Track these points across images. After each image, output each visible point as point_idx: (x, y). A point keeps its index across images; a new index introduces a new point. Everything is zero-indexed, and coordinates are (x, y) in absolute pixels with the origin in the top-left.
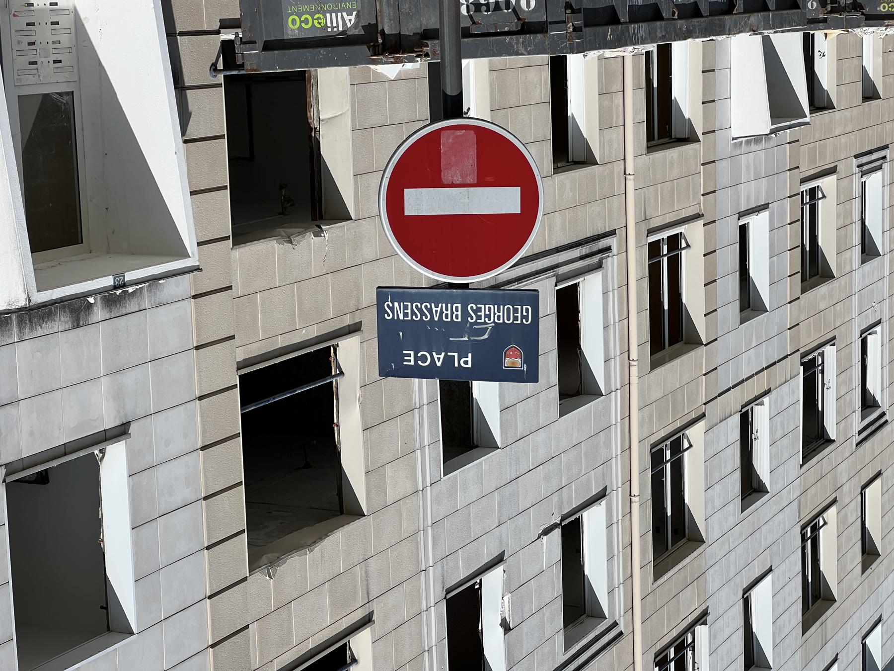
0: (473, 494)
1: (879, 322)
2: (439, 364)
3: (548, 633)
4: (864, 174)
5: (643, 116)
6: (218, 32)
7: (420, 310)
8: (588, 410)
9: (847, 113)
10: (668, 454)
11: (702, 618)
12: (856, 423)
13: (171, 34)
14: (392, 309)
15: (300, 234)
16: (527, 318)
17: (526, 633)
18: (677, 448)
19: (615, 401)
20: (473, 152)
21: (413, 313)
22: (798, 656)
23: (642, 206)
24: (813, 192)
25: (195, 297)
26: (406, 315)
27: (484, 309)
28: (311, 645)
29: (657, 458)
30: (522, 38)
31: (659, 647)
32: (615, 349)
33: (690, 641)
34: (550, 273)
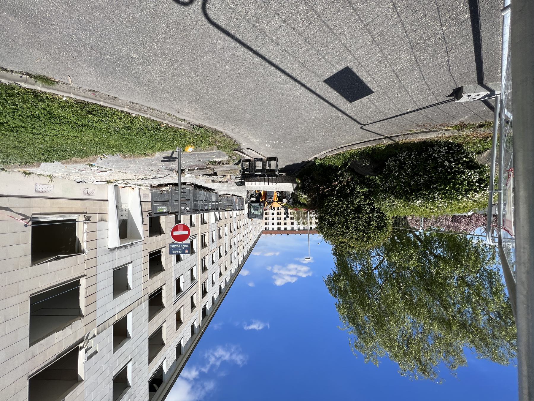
0: (179, 266)
3: (189, 282)
11: (207, 279)
13: (142, 212)
17: (186, 283)
18: (204, 259)
27: (183, 246)
29: (202, 260)
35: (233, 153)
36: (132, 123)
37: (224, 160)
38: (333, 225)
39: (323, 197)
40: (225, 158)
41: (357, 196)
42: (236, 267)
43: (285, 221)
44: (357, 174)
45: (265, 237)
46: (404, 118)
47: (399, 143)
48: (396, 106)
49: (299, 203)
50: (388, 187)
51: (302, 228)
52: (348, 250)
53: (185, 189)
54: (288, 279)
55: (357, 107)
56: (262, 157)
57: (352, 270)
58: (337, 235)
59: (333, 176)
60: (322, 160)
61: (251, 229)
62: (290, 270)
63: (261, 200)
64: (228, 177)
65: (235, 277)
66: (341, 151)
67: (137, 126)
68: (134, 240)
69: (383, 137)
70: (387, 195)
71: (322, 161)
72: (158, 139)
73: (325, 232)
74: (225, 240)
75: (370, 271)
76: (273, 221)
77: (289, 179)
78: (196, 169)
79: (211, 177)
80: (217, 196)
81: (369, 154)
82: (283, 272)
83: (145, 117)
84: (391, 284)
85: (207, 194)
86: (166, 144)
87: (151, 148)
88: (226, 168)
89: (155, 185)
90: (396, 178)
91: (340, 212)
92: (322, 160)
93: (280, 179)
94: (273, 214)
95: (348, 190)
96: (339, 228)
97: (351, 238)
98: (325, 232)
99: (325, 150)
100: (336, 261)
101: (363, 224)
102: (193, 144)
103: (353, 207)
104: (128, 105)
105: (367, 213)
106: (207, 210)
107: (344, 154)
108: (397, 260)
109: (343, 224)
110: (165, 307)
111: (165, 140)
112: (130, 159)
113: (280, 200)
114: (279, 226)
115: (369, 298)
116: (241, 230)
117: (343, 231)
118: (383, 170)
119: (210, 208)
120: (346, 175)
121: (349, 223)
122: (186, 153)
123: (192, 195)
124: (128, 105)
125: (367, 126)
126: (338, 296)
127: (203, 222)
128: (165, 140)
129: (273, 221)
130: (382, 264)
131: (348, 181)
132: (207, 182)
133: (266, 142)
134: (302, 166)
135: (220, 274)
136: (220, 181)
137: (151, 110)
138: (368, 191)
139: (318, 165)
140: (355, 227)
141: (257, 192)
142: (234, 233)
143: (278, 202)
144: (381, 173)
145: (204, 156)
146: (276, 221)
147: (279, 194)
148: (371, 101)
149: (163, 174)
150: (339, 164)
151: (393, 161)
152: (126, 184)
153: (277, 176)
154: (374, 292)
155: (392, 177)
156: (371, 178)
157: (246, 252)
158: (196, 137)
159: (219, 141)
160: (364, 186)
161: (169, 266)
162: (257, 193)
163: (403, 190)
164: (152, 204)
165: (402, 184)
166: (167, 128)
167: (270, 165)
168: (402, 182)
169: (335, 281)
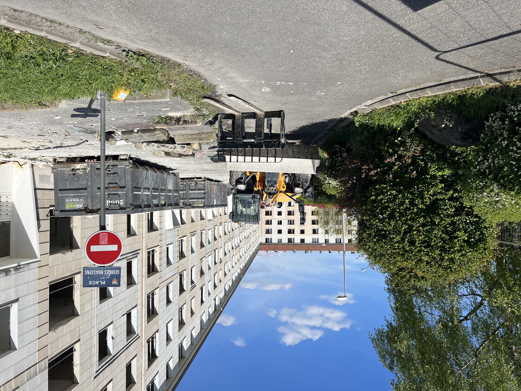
0: (106, 308)
1: (194, 266)
2: (97, 284)
3: (123, 338)
4: (192, 236)
5: (147, 225)
6: (49, 208)
7: (93, 272)
8: (133, 288)
9: (188, 225)
10: (151, 296)
11: (157, 331)
12: (190, 286)
13: (37, 208)
14: (87, 272)
15: (67, 252)
16: (118, 273)
17: (117, 340)
18: (153, 294)
19: (139, 285)
20: (107, 238)
21: (92, 273)
22: (178, 337)
23: (146, 244)
24: (182, 240)
25: (39, 267)
26: (90, 273)
27: (108, 271)
28: (64, 348)
29: (148, 297)
30: (120, 210)
31: (148, 339)
32: (140, 274)
33: (155, 336)
34: (126, 259)
35: (202, 103)
36: (13, 47)
37: (187, 115)
38: (385, 236)
39: (369, 183)
40: (189, 112)
41: (431, 183)
42: (211, 310)
43: (302, 227)
44: (432, 142)
45: (265, 255)
46: (515, 39)
47: (509, 86)
48: (500, 19)
49: (325, 194)
50: (489, 167)
51: (332, 240)
52: (413, 282)
53: (115, 168)
54: (308, 334)
55: (426, 19)
56: (257, 111)
57: (422, 318)
58: (392, 255)
59: (388, 147)
60: (366, 116)
61: (239, 241)
62: (310, 318)
63: (256, 189)
64: (196, 146)
65: (209, 328)
66: (402, 101)
67: (22, 51)
68: (24, 259)
69: (478, 74)
70: (486, 183)
71: (367, 118)
72: (62, 75)
73: (370, 250)
74: (191, 259)
75: (456, 323)
76: (280, 227)
77: (306, 150)
78: (135, 131)
79: (163, 146)
80: (176, 180)
81: (453, 106)
82: (298, 321)
83: (37, 35)
84: (497, 348)
85: (157, 177)
86: (78, 85)
87: (51, 92)
88: (190, 130)
89: (62, 160)
90: (504, 151)
91: (398, 212)
92: (366, 116)
93: (290, 152)
94: (280, 213)
95: (415, 172)
96: (396, 243)
97: (419, 260)
98: (370, 250)
99: (371, 99)
100: (392, 304)
101: (441, 236)
102: (127, 85)
103: (423, 203)
104: (6, 14)
105: (448, 216)
106: (157, 205)
107: (408, 105)
108: (507, 303)
109: (403, 235)
110: (77, 383)
111: (75, 77)
112: (13, 112)
113: (290, 189)
114: (291, 236)
115: (452, 372)
116: (220, 242)
117: (403, 248)
118: (480, 135)
119: (163, 202)
120: (410, 145)
121: (415, 233)
122: (116, 102)
123: (129, 178)
124: (6, 14)
125: (448, 53)
126: (395, 368)
127: (151, 227)
128: (75, 77)
129: (280, 227)
130: (478, 311)
131: (414, 155)
132: (156, 155)
133: (261, 83)
134: (329, 127)
135: (182, 324)
136: (181, 153)
137: (48, 23)
138: (452, 175)
139: (360, 125)
140: (425, 242)
141: (248, 174)
142: (208, 247)
143: (288, 194)
144: (476, 141)
145: (149, 107)
146: (285, 227)
147: (287, 179)
148: (453, 8)
149: (75, 139)
150: (397, 123)
151: (498, 120)
152: (9, 157)
153: (283, 146)
154: (463, 363)
155: (496, 149)
156: (459, 150)
157: (230, 283)
158: (133, 74)
159: (175, 80)
160: (444, 164)
161: (88, 307)
162: (248, 176)
163: (516, 174)
164: (56, 195)
165: (514, 163)
166: (78, 56)
167: (270, 126)
168: (514, 159)
169: (391, 341)
